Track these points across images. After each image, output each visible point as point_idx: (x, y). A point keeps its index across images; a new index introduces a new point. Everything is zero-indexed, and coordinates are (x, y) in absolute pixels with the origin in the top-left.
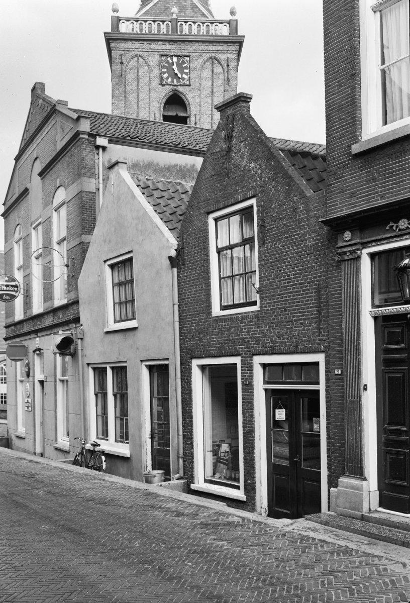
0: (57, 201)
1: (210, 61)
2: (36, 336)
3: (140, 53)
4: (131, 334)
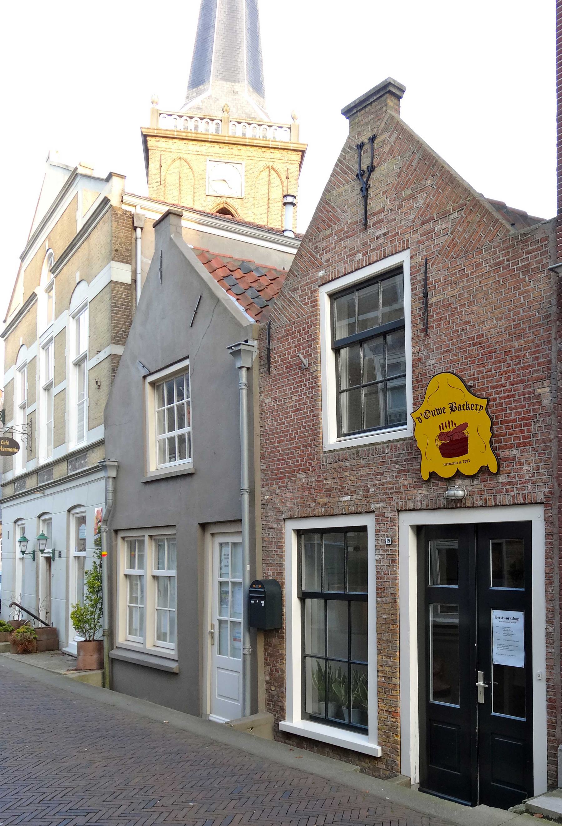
0: (76, 302)
1: (267, 171)
2: (42, 495)
3: (186, 156)
4: (188, 480)
